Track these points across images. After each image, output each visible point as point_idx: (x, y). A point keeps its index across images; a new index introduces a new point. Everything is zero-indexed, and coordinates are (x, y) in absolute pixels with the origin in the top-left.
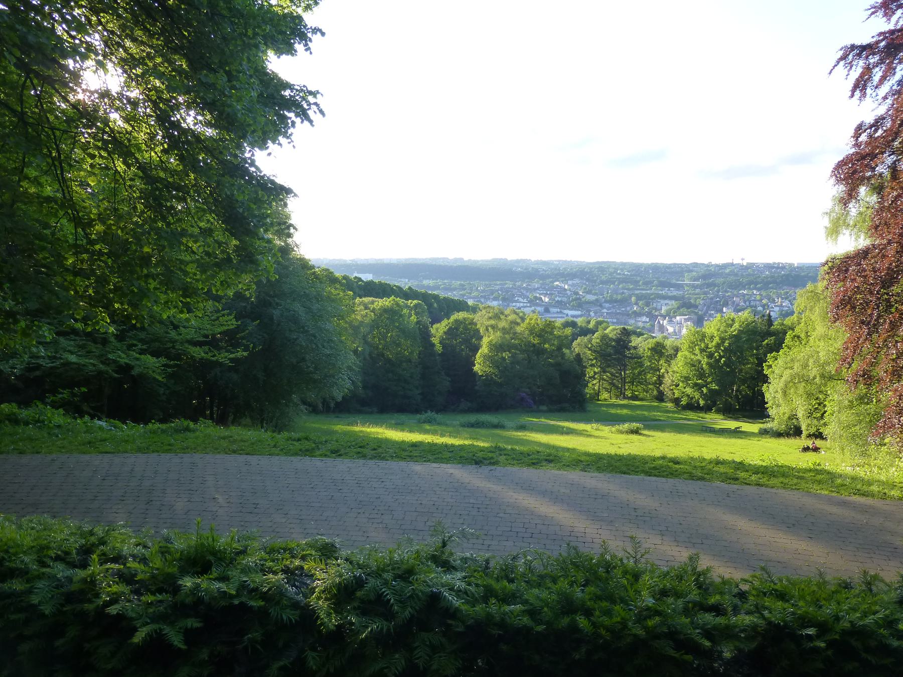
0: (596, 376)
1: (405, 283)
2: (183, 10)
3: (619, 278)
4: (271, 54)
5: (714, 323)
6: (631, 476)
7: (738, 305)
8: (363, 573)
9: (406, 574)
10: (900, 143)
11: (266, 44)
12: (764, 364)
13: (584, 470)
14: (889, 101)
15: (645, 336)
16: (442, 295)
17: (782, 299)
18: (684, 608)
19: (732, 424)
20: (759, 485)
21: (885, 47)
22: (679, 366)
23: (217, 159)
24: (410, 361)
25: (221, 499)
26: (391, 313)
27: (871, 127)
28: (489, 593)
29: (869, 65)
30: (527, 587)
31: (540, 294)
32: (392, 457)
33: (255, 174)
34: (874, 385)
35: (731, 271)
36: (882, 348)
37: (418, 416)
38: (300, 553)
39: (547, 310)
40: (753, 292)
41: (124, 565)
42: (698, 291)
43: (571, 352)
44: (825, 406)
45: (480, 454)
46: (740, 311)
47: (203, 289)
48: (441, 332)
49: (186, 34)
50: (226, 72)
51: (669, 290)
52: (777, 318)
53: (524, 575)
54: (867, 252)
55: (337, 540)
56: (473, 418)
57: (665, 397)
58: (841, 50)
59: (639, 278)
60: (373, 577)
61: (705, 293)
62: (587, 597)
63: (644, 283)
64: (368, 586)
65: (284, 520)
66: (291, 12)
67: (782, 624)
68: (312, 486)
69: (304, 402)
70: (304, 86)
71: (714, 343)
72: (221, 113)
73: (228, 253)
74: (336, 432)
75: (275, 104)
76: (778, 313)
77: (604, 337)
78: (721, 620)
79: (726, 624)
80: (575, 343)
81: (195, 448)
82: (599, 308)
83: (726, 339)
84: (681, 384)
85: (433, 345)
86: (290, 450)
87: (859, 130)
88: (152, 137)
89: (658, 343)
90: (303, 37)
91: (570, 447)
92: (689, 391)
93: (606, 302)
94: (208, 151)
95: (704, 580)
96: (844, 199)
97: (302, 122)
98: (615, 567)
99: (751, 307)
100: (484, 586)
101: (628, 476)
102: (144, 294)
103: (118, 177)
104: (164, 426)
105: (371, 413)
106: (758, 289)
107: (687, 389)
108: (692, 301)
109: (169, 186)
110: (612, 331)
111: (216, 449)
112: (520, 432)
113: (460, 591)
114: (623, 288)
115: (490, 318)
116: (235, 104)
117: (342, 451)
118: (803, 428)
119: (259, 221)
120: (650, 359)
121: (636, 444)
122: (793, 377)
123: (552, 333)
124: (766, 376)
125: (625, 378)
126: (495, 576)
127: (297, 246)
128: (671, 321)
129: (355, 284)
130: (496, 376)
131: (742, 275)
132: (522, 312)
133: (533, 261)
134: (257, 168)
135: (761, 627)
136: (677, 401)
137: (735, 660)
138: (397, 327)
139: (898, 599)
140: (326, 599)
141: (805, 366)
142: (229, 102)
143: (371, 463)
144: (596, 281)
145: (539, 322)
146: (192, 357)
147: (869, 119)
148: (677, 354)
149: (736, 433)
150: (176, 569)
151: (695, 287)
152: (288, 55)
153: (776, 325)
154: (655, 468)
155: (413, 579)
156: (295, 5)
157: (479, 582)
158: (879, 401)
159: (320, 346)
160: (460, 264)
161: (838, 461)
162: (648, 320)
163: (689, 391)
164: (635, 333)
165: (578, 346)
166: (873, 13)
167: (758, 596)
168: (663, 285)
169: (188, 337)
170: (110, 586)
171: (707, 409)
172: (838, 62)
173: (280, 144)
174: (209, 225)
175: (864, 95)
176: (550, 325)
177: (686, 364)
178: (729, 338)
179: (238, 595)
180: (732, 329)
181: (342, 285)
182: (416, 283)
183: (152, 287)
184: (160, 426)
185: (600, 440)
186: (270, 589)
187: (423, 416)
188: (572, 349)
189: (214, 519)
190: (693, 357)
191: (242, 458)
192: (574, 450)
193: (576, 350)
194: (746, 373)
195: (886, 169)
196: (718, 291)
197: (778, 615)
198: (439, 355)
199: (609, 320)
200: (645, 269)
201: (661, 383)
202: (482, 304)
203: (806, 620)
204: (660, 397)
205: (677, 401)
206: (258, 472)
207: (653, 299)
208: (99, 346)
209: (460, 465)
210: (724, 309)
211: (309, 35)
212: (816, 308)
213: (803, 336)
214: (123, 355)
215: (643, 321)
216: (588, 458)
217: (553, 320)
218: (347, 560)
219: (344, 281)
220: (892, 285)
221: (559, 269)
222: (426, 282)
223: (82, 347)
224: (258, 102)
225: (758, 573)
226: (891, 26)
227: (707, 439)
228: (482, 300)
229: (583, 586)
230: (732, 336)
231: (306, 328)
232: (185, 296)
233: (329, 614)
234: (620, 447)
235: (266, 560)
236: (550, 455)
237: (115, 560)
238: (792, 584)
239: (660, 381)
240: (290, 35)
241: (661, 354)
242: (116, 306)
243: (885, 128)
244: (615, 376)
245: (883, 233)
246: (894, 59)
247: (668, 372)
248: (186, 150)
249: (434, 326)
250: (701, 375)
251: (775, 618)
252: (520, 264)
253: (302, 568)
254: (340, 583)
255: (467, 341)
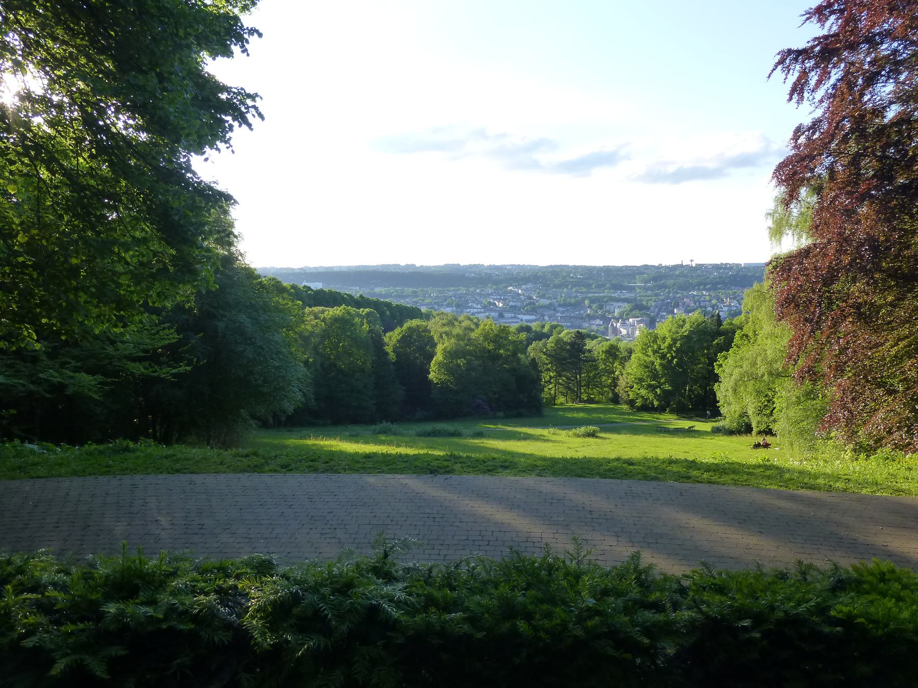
0: (552, 381)
1: (356, 291)
2: (109, 7)
3: (572, 282)
4: (205, 54)
5: (666, 324)
6: (587, 479)
7: (689, 306)
8: (300, 589)
9: (345, 587)
10: (836, 145)
11: (199, 44)
12: (715, 364)
13: (539, 475)
14: (825, 105)
15: (599, 339)
16: (395, 302)
17: (731, 299)
18: (624, 607)
19: (685, 424)
20: (710, 482)
21: (820, 51)
22: (633, 367)
23: (150, 165)
24: (363, 371)
25: (164, 521)
26: (343, 323)
27: (809, 130)
28: (430, 601)
29: (805, 69)
30: (468, 595)
31: (494, 300)
32: (345, 469)
33: (191, 180)
34: (819, 380)
35: (680, 273)
36: (826, 345)
37: (373, 427)
38: (234, 572)
39: (501, 316)
40: (702, 293)
41: (43, 594)
42: (649, 292)
43: (527, 357)
44: (774, 403)
45: (435, 463)
46: (689, 312)
47: (138, 301)
48: (394, 340)
49: (113, 33)
50: (158, 75)
51: (621, 292)
52: (726, 318)
53: (466, 582)
54: (808, 251)
55: (275, 556)
56: (429, 427)
57: (620, 399)
58: (778, 54)
59: (591, 282)
60: (310, 592)
61: (656, 295)
62: (528, 601)
63: (596, 287)
64: (304, 603)
65: (231, 540)
66: (227, 12)
67: (719, 617)
68: (260, 503)
69: (254, 417)
70: (242, 89)
71: (666, 344)
72: (152, 116)
73: (164, 263)
74: (287, 447)
75: (210, 107)
76: (727, 313)
77: (559, 341)
78: (660, 617)
79: (665, 621)
80: (530, 348)
81: (135, 469)
82: (552, 312)
83: (678, 340)
84: (635, 386)
85: (387, 354)
86: (238, 466)
87: (798, 131)
88: (79, 140)
89: (612, 345)
90: (241, 40)
91: (528, 452)
92: (643, 392)
93: (560, 305)
94: (138, 155)
95: (646, 578)
96: (785, 200)
97: (240, 126)
98: (557, 570)
99: (701, 307)
100: (424, 595)
101: (583, 479)
102: (73, 307)
103: (41, 184)
104: (101, 447)
105: (324, 425)
106: (707, 290)
107: (641, 391)
108: (644, 303)
109: (99, 195)
110: (566, 334)
111: (158, 469)
112: (477, 439)
113: (400, 602)
114: (577, 292)
115: (444, 325)
116: (167, 106)
117: (293, 465)
118: (754, 425)
119: (197, 229)
120: (605, 361)
121: (593, 447)
122: (742, 376)
123: (506, 338)
124: (717, 376)
125: (580, 381)
126: (438, 584)
127: (241, 255)
128: (624, 323)
129: (304, 293)
130: (451, 383)
131: (692, 276)
132: (476, 318)
133: (486, 265)
134: (194, 173)
135: (699, 621)
136: (631, 403)
137: (677, 656)
138: (349, 336)
139: (831, 587)
140: (261, 618)
141: (754, 364)
142: (160, 104)
143: (323, 476)
144: (549, 285)
145: (493, 327)
146: (132, 374)
147: (807, 121)
148: (631, 356)
149: (690, 433)
150: (99, 595)
151: (646, 289)
152: (224, 57)
153: (725, 325)
154: (610, 470)
155: (352, 593)
156: (231, 5)
157: (420, 592)
158: (824, 396)
159: (269, 359)
160: (412, 271)
161: (788, 456)
162: (601, 323)
163: (643, 392)
164: (589, 336)
165: (534, 350)
166: (808, 19)
167: (698, 590)
168: (616, 287)
169: (126, 353)
170: (26, 617)
171: (661, 410)
172: (776, 66)
173: (218, 149)
174: (143, 234)
175: (801, 98)
176: (504, 331)
177: (640, 365)
178: (680, 339)
179: (166, 619)
180: (683, 330)
181: (290, 294)
182: (368, 291)
183: (82, 300)
184: (97, 447)
185: (557, 444)
186: (201, 611)
187: (378, 427)
188: (528, 354)
189: (157, 542)
190: (646, 358)
191: (185, 478)
192: (531, 455)
193: (532, 355)
194: (698, 373)
195: (824, 171)
196: (669, 293)
197: (715, 610)
198: (394, 364)
199: (563, 324)
200: (597, 272)
201: (616, 385)
202: (436, 310)
203: (743, 612)
204: (616, 400)
205: (631, 403)
206: (204, 491)
207: (606, 302)
208: (29, 365)
209: (415, 475)
210: (675, 310)
211: (246, 36)
212: (763, 307)
213: (750, 334)
214: (56, 374)
215: (596, 325)
216: (543, 463)
217: (508, 325)
218: (282, 577)
219: (292, 290)
220: (832, 283)
221: (512, 275)
222: (377, 290)
223: (10, 366)
224: (193, 105)
225: (699, 568)
226: (825, 32)
227: (662, 439)
228: (436, 307)
229: (525, 589)
230: (683, 337)
231: (253, 340)
232: (118, 309)
233: (263, 634)
234: (577, 451)
235: (198, 581)
236: (506, 461)
237: (32, 590)
238: (730, 577)
239: (615, 384)
240: (225, 35)
241: (615, 357)
242: (44, 321)
243: (822, 131)
244: (570, 380)
245: (824, 232)
246: (828, 64)
247: (622, 375)
248: (116, 156)
249: (387, 334)
250: (655, 376)
251: (714, 612)
252: (474, 270)
253: (236, 587)
254: (275, 601)
255: (421, 349)
